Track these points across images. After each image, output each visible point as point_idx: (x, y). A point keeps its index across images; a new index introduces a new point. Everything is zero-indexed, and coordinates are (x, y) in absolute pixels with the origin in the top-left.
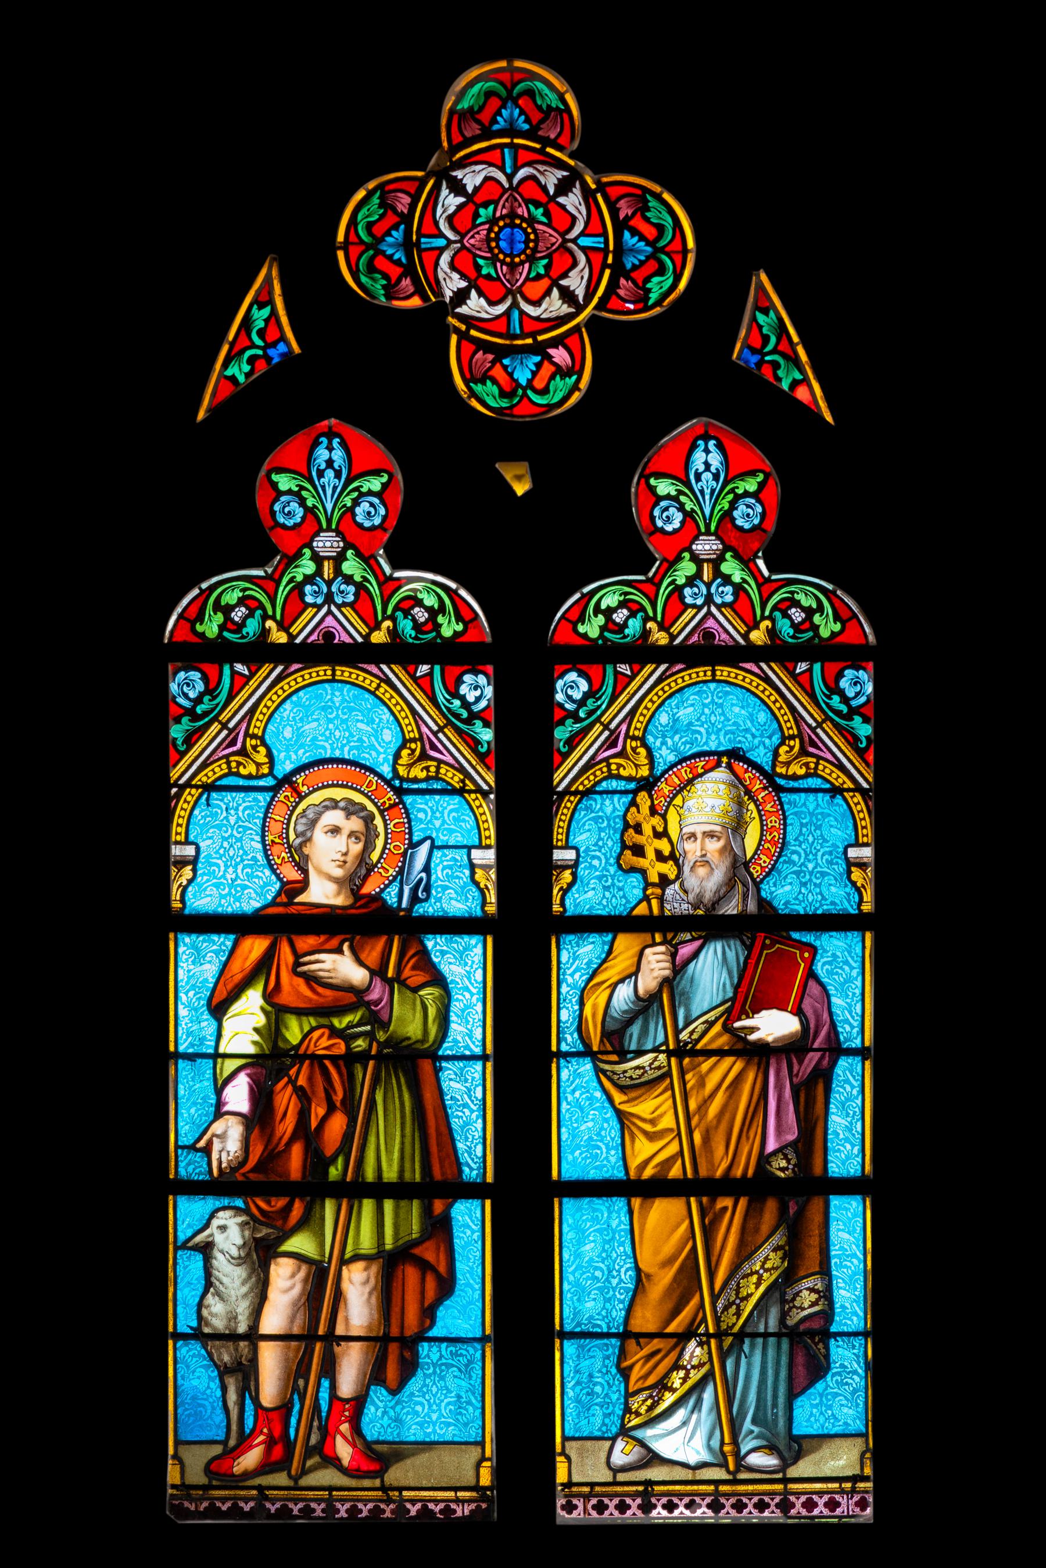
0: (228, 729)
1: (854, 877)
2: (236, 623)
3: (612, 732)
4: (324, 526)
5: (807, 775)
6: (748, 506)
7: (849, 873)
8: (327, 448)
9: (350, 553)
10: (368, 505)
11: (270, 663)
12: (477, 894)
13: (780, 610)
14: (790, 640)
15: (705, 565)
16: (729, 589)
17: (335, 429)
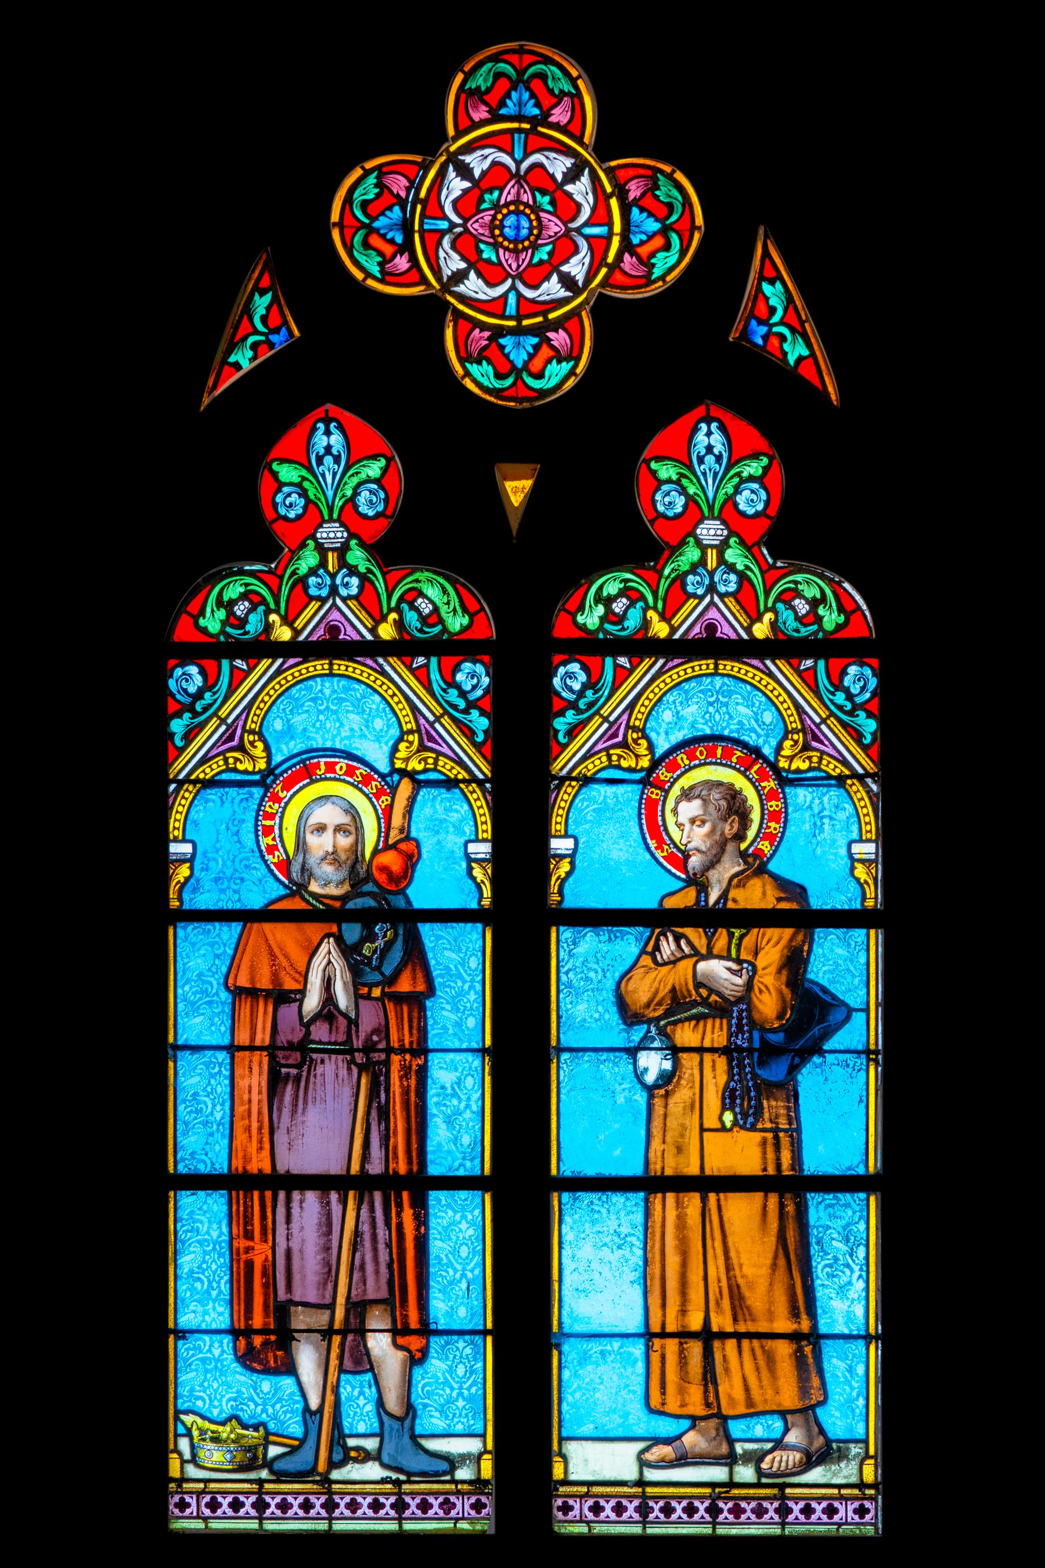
0: (609, 722)
1: (857, 873)
2: (238, 618)
3: (229, 727)
4: (326, 517)
5: (425, 771)
6: (753, 492)
7: (852, 869)
8: (324, 433)
9: (733, 540)
10: (368, 493)
11: (268, 658)
12: (473, 887)
13: (785, 602)
14: (419, 635)
15: (709, 551)
16: (733, 577)
17: (331, 415)
